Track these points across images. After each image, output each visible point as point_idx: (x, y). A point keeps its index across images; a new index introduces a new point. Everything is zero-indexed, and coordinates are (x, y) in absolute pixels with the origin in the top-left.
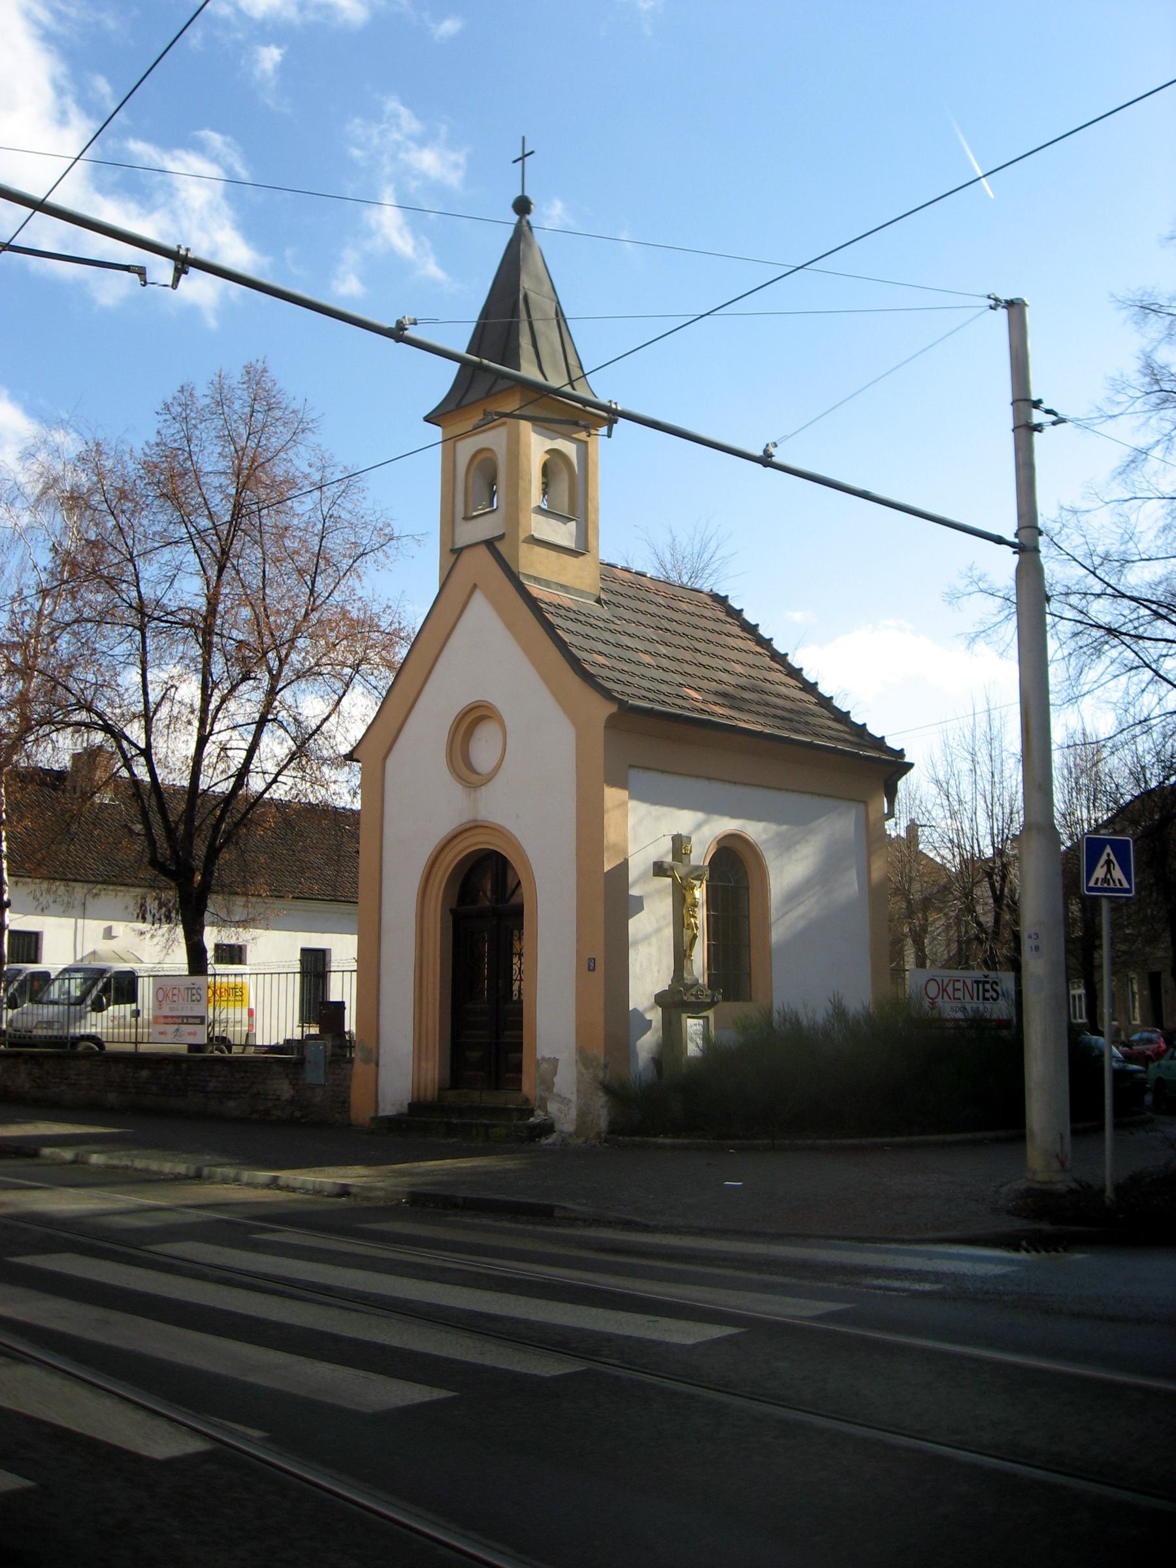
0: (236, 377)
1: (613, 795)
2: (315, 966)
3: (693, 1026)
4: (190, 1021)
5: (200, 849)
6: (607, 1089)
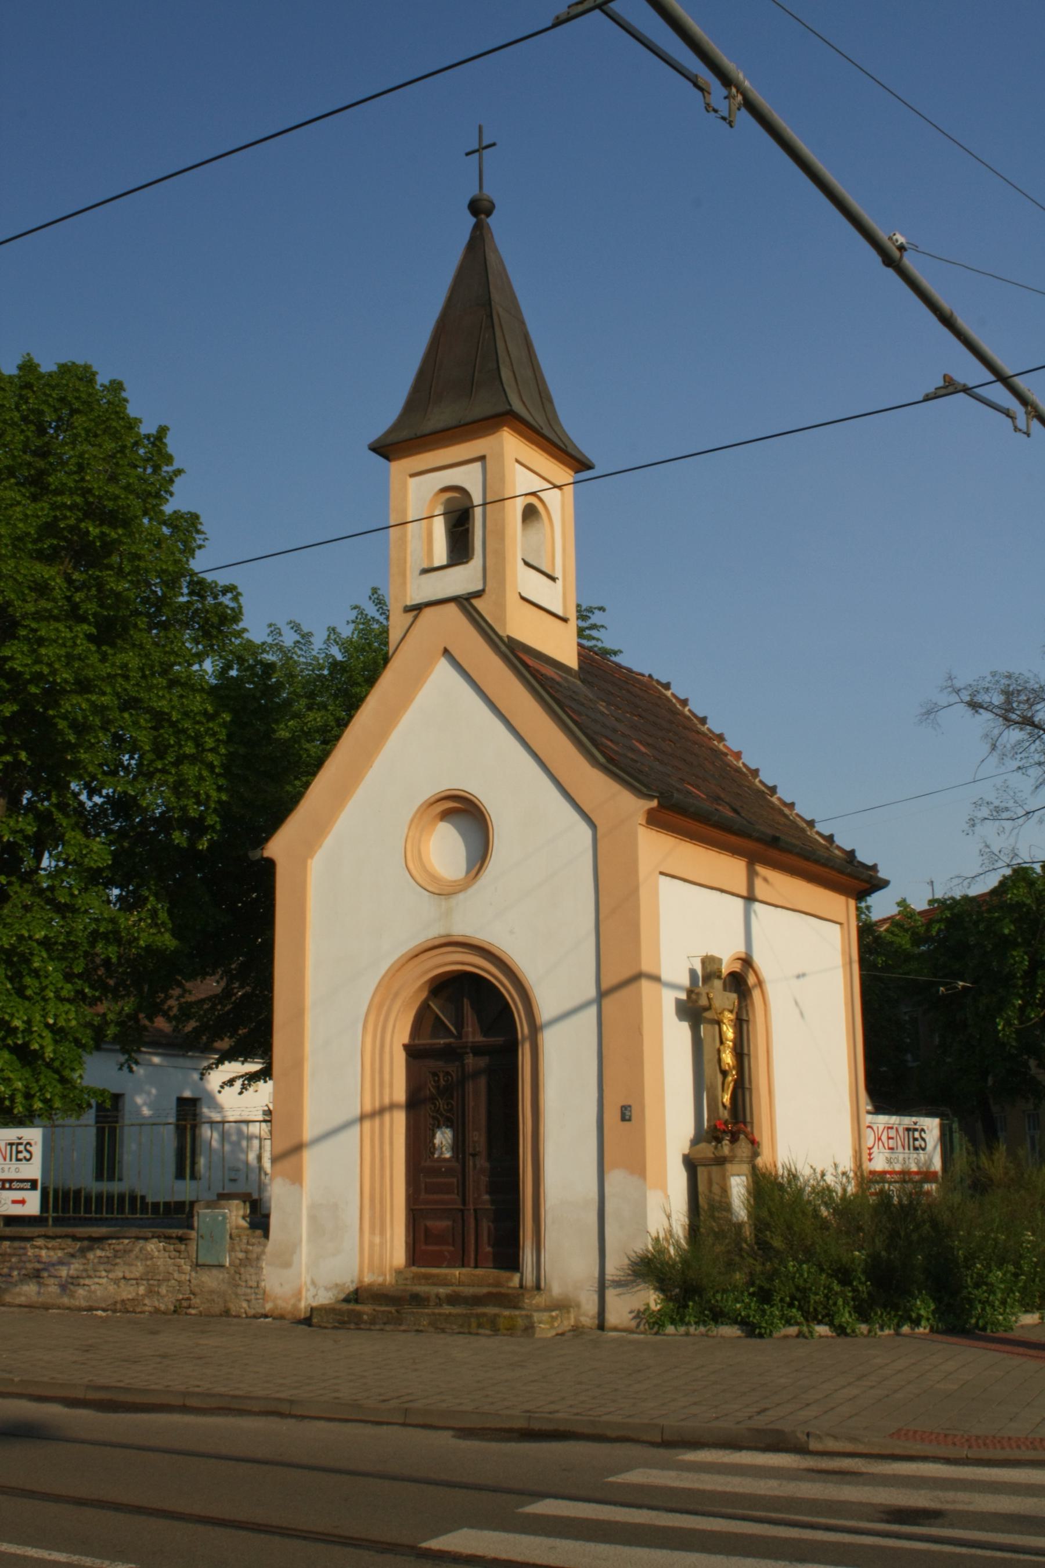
4: (15, 1185)
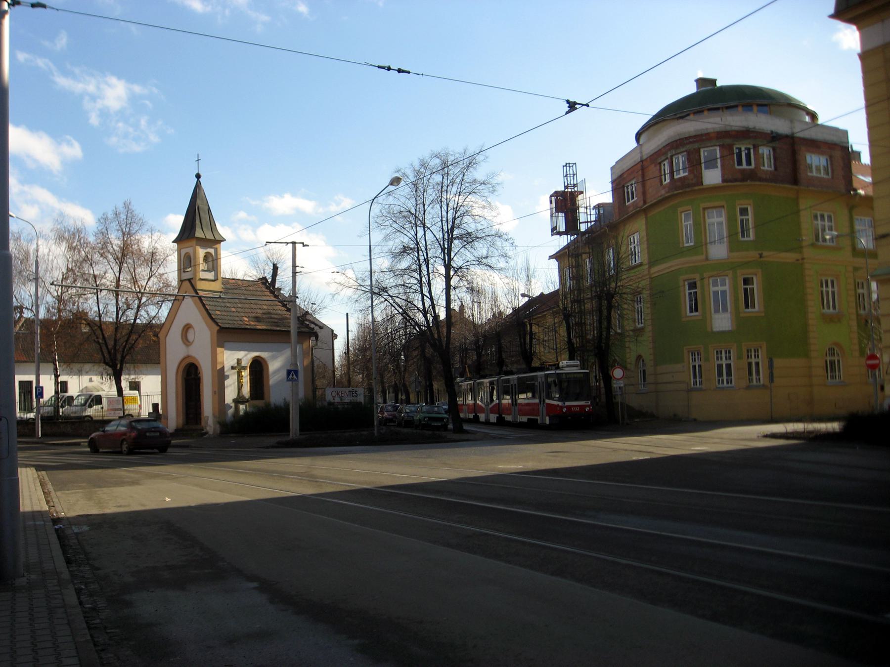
0: (121, 208)
1: (219, 350)
2: (258, 368)
3: (242, 407)
5: (119, 357)
6: (219, 423)
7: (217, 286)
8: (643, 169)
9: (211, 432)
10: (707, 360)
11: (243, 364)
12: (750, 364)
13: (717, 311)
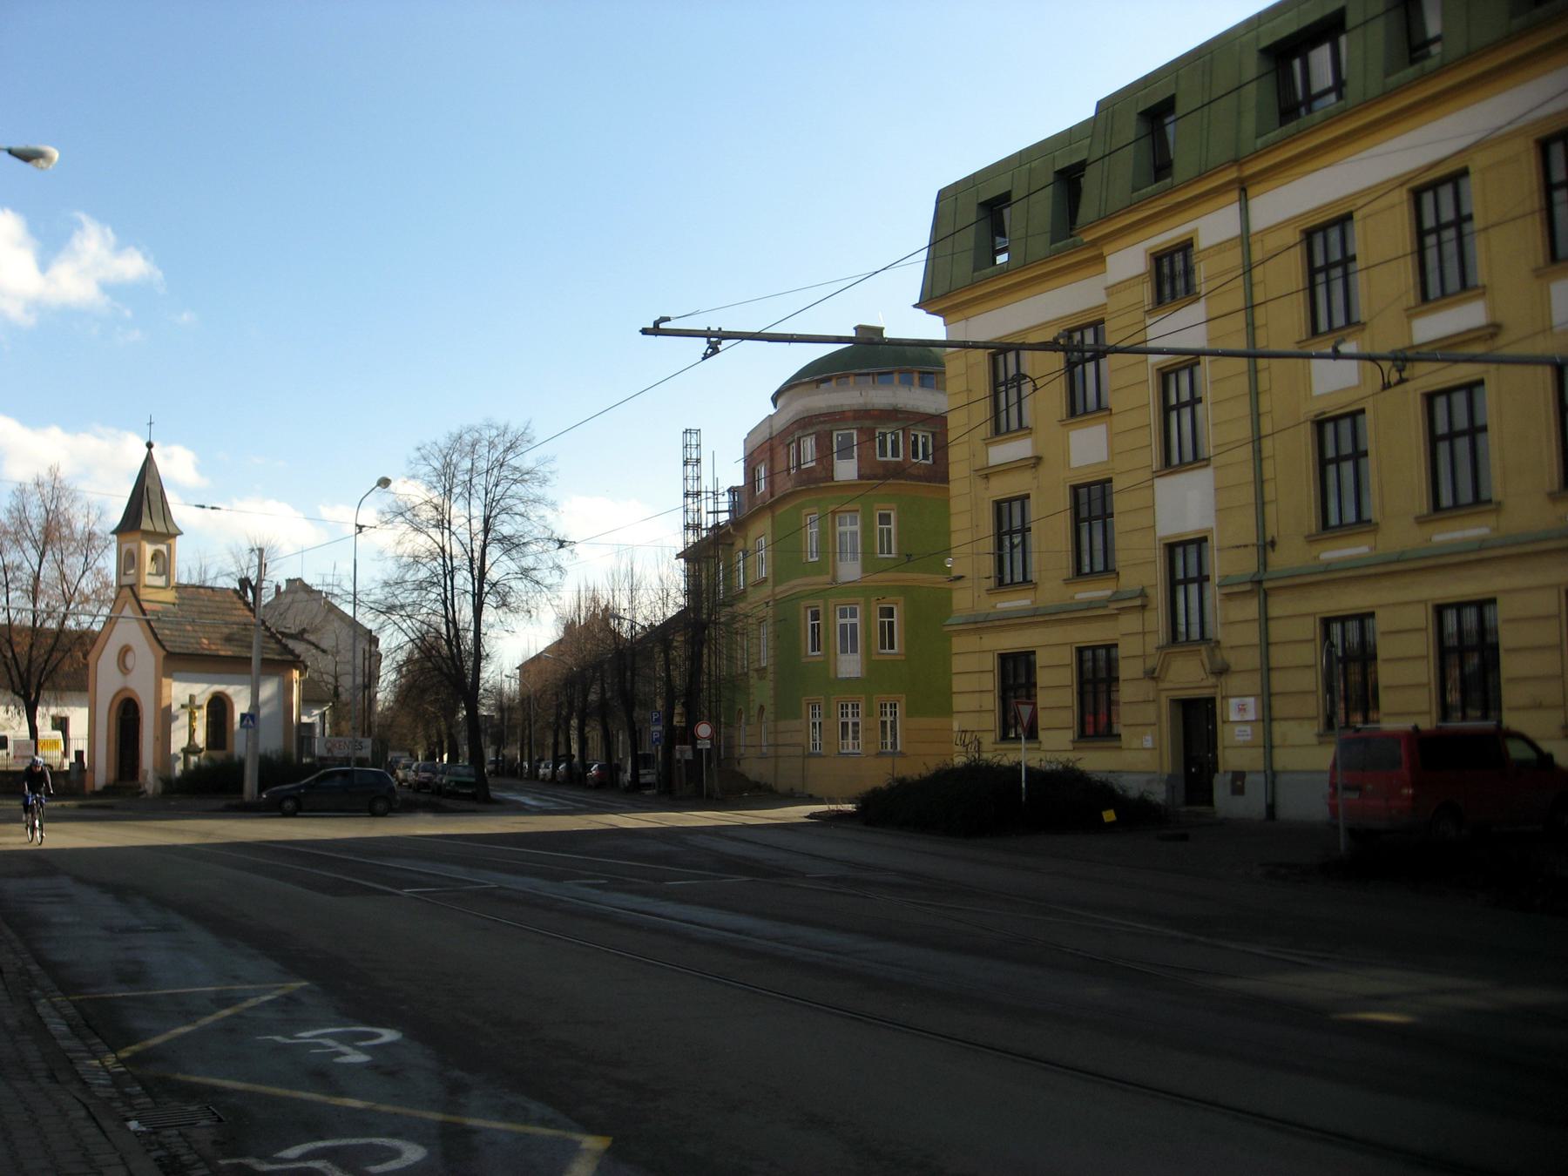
1: (165, 681)
2: (219, 706)
3: (193, 759)
5: (34, 681)
6: (161, 779)
7: (170, 596)
8: (772, 450)
9: (150, 791)
10: (828, 716)
11: (198, 702)
12: (884, 723)
13: (844, 651)
